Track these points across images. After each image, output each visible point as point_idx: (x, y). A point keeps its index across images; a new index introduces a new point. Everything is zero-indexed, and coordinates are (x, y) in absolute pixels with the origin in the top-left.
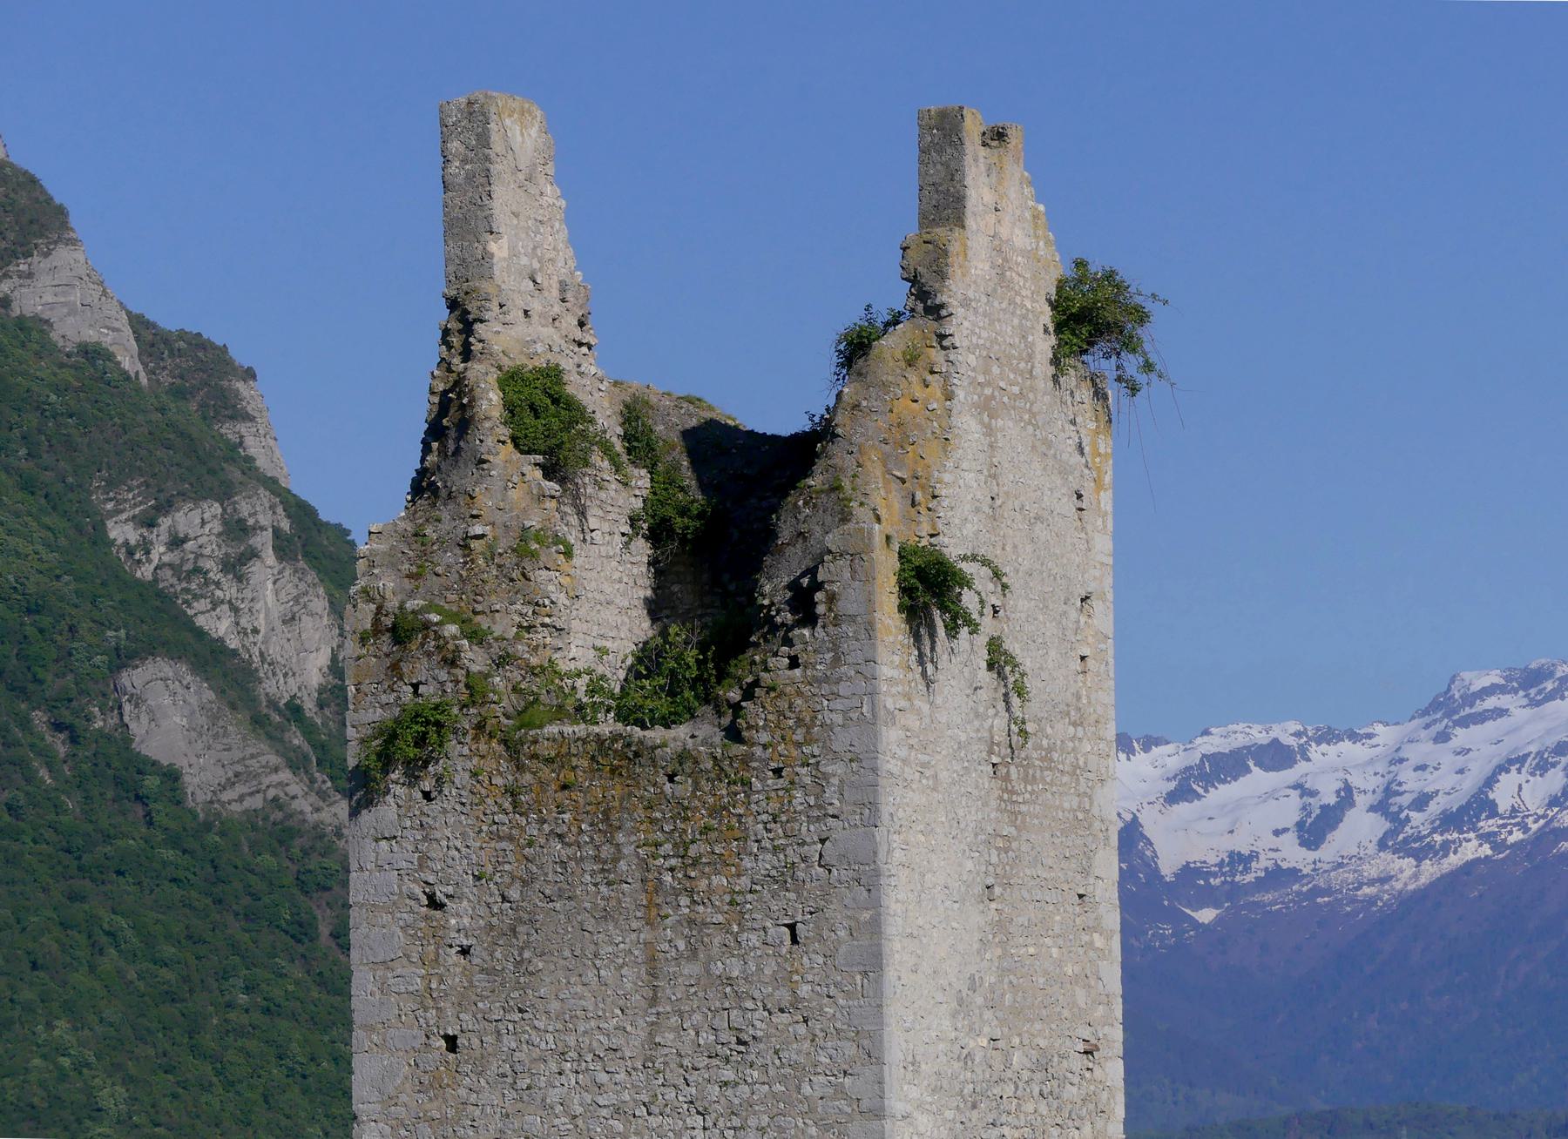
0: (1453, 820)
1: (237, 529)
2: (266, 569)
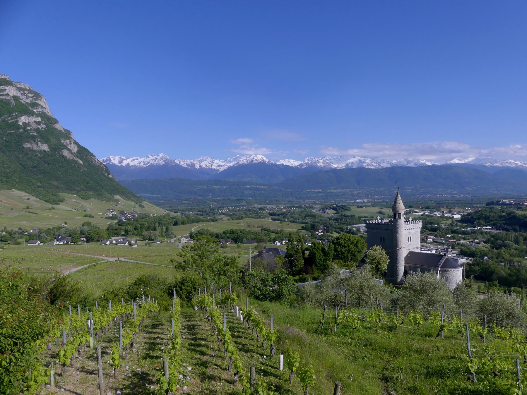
0: (147, 163)
1: (70, 142)
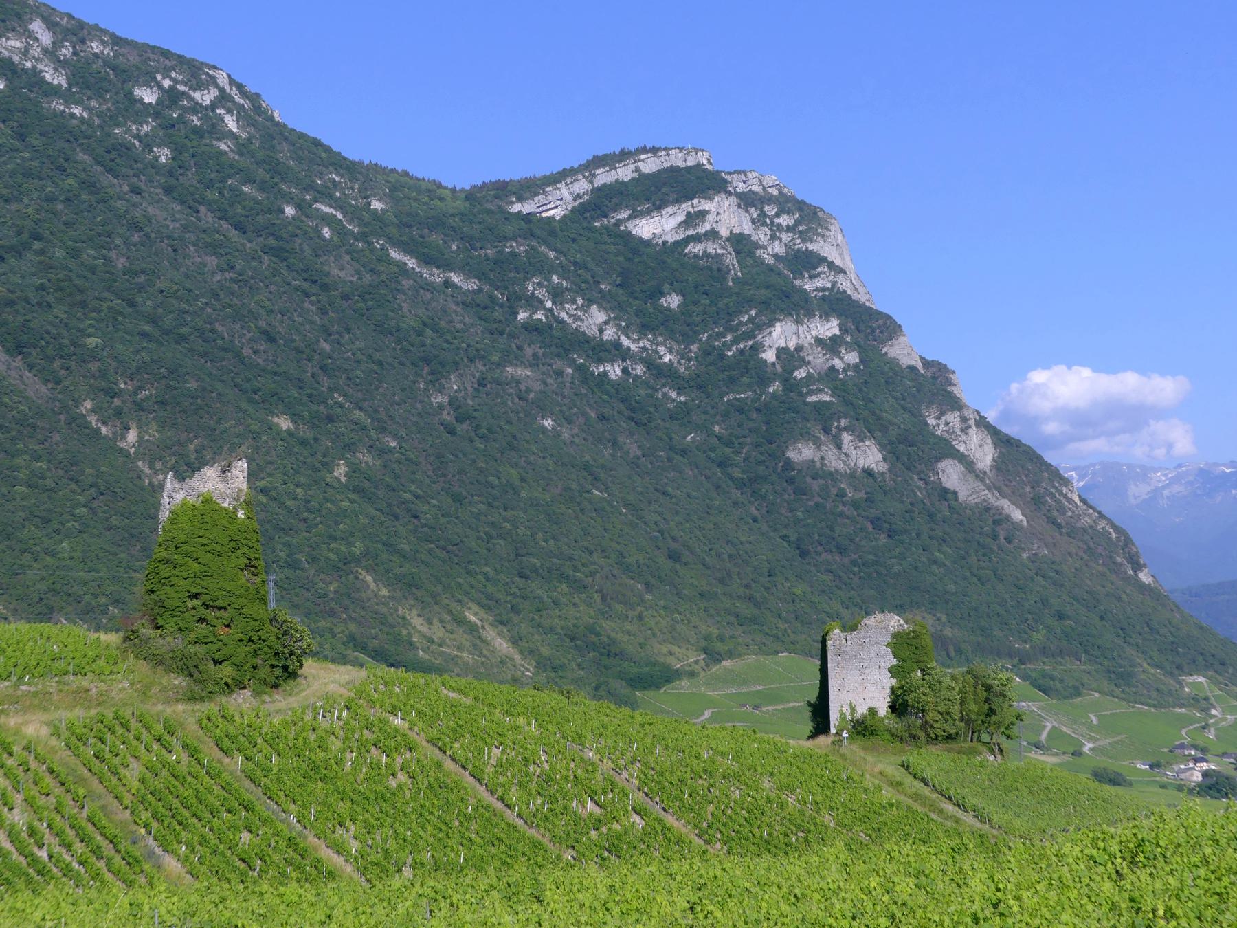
1: (964, 419)
2: (973, 431)
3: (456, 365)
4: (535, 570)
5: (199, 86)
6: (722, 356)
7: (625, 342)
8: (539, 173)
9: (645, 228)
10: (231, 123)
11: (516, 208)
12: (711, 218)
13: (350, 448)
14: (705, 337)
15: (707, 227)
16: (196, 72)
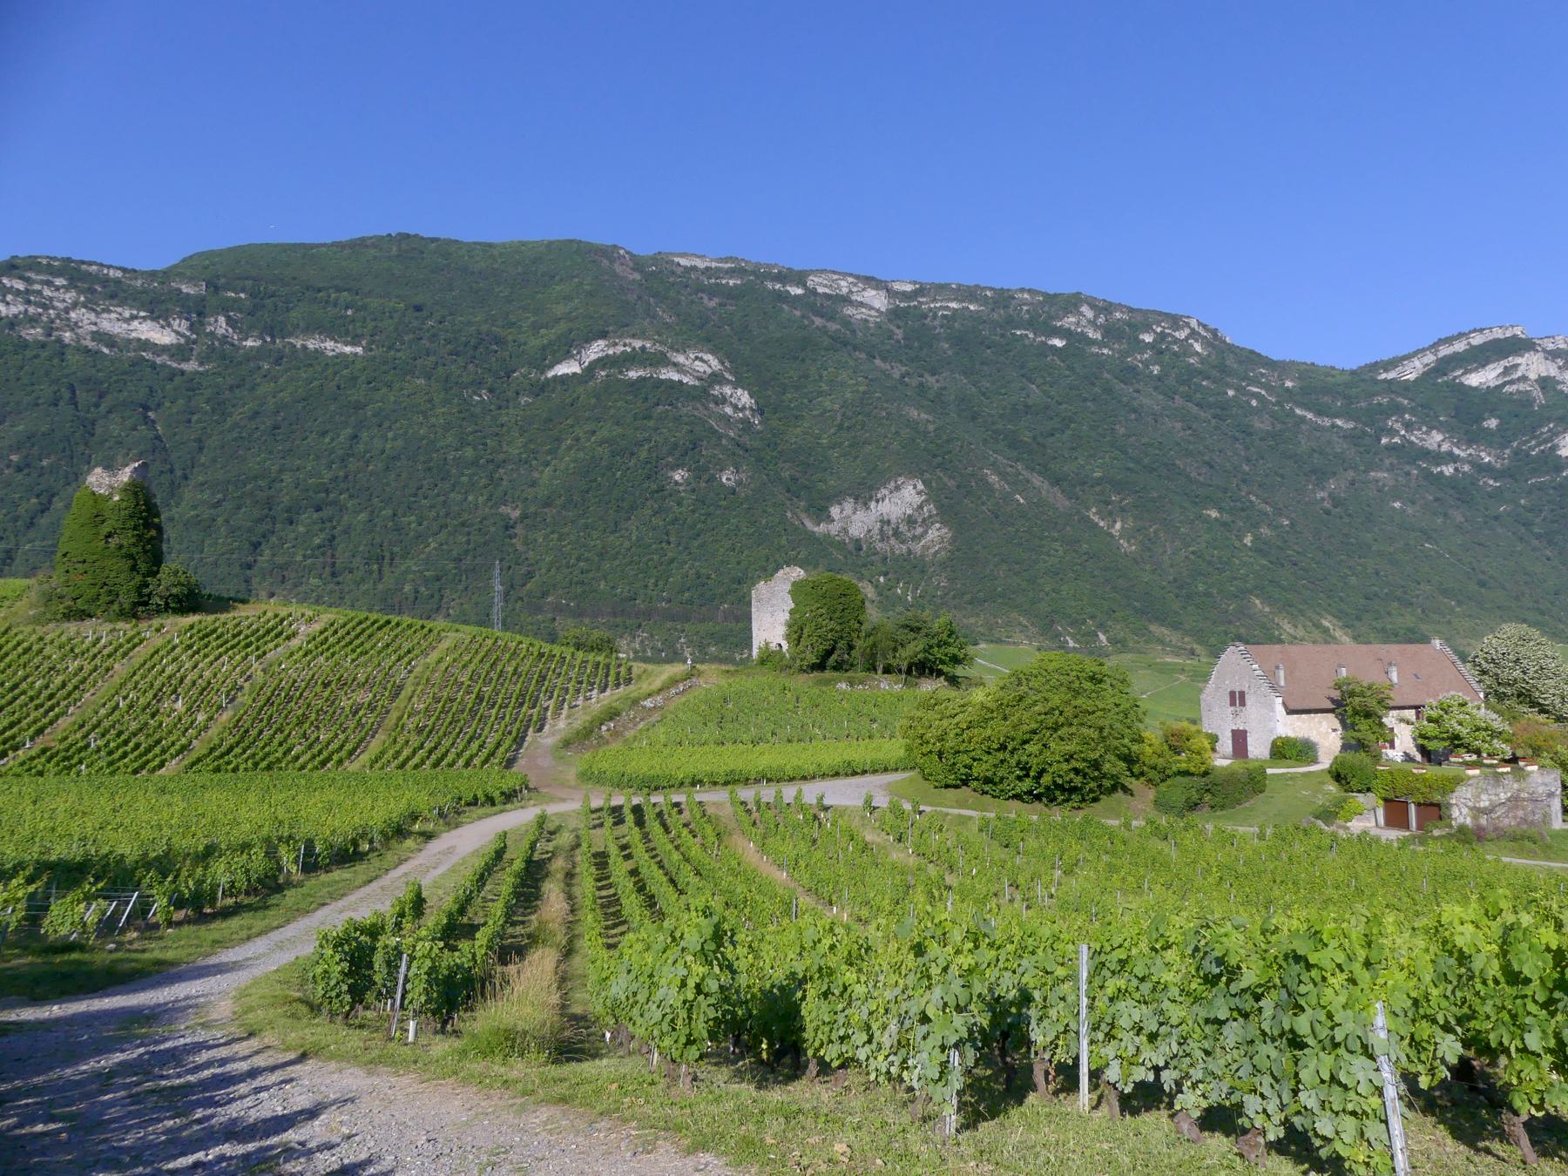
3: (1334, 474)
4: (1376, 595)
5: (1178, 329)
6: (1528, 455)
7: (1456, 451)
8: (1401, 354)
9: (1474, 380)
10: (1198, 347)
11: (1383, 376)
12: (1522, 368)
13: (1256, 525)
14: (1515, 444)
15: (1519, 374)
16: (1176, 321)
